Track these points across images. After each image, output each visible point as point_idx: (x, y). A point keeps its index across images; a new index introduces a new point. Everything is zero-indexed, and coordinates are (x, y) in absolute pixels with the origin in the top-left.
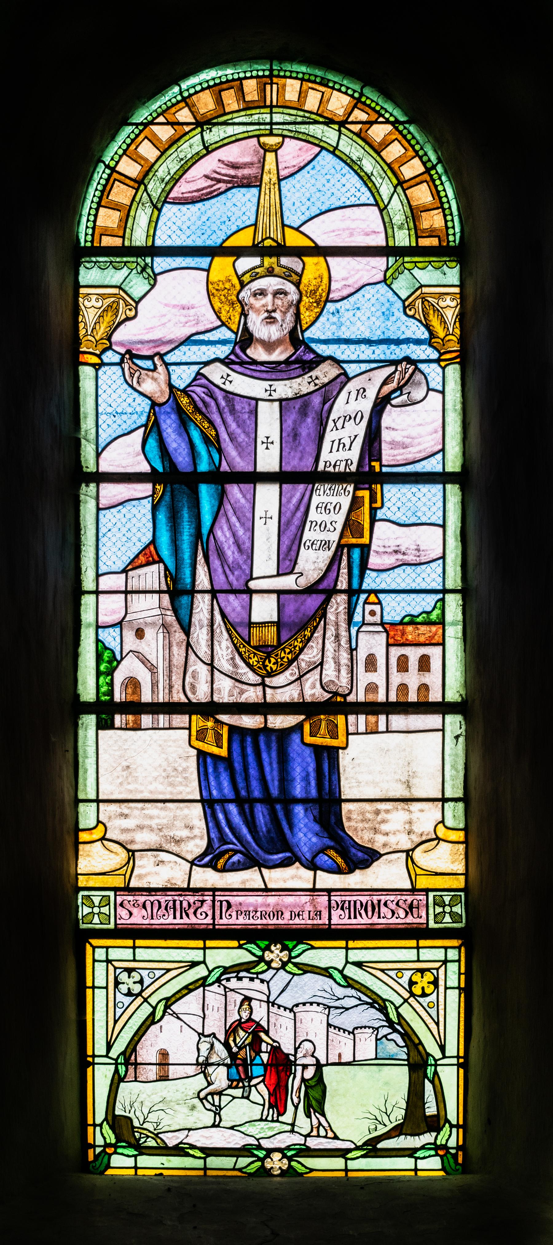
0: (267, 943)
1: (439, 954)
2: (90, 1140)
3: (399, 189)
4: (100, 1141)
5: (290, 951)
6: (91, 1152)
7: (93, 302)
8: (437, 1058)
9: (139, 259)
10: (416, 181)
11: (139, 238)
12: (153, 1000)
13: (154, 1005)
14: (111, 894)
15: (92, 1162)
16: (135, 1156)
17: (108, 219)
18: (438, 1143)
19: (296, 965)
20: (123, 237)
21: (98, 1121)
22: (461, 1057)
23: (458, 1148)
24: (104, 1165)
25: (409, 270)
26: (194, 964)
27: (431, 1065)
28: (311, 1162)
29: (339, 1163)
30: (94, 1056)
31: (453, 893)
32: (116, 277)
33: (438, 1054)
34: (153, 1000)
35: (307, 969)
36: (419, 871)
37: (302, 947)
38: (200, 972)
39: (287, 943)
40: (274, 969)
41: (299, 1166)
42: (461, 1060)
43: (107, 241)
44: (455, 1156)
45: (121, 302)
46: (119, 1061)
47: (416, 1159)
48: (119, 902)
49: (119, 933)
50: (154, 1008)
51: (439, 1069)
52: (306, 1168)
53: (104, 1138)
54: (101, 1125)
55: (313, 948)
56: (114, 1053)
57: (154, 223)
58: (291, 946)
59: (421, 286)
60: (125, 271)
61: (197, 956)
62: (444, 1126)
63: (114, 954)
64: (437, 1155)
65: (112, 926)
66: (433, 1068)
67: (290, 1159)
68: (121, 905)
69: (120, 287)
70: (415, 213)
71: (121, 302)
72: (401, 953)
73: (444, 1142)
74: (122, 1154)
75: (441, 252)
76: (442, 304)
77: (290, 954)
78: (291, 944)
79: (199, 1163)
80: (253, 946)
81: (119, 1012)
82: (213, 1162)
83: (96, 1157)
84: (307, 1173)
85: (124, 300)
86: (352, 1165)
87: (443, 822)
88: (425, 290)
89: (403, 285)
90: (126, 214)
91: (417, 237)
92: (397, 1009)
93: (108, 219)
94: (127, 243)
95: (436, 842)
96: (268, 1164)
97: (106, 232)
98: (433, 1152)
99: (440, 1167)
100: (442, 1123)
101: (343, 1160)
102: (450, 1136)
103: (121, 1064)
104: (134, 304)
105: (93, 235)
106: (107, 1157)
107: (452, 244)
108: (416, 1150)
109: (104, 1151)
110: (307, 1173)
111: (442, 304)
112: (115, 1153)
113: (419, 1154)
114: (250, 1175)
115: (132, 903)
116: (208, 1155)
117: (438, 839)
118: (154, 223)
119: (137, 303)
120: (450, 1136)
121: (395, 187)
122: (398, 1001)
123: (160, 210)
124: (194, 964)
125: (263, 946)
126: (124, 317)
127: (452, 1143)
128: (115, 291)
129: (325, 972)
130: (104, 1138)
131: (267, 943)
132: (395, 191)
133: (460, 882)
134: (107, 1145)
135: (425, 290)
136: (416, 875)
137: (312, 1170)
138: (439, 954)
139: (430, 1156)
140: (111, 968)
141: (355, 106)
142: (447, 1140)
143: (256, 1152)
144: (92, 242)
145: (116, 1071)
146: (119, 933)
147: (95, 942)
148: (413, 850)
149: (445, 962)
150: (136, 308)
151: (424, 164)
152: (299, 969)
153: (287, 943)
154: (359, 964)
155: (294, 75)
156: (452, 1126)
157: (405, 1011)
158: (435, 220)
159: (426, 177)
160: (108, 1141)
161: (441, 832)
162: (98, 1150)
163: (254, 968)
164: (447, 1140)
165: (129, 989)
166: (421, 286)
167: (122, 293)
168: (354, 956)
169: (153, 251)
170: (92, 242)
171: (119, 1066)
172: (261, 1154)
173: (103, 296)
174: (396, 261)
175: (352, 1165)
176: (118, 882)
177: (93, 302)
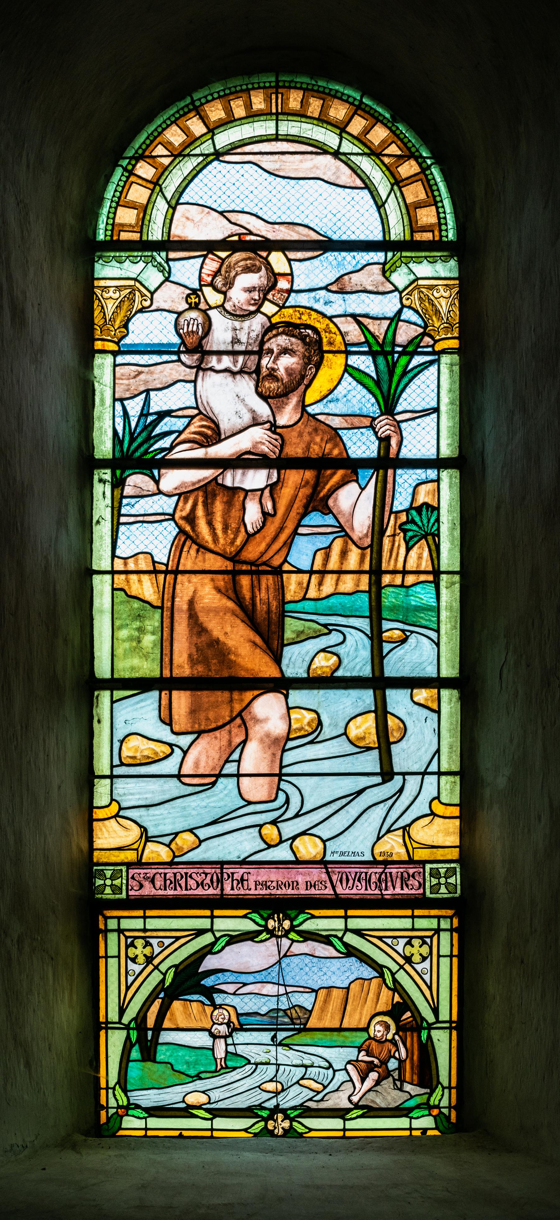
0: (269, 912)
1: (433, 923)
2: (103, 1102)
3: (395, 188)
4: (112, 1103)
5: (292, 921)
6: (103, 1113)
7: (111, 294)
8: (430, 1021)
9: (155, 253)
10: (412, 179)
11: (156, 234)
12: (163, 967)
13: (164, 971)
14: (124, 869)
15: (104, 1124)
16: (145, 1118)
17: (126, 216)
18: (431, 1103)
19: (299, 933)
20: (141, 232)
21: (112, 1084)
22: (454, 1022)
23: (450, 1107)
24: (117, 1126)
25: (406, 264)
26: (200, 932)
27: (425, 1029)
28: (311, 1123)
29: (337, 1123)
30: (107, 1022)
31: (448, 866)
32: (131, 269)
33: (431, 1018)
34: (163, 967)
35: (308, 936)
36: (415, 845)
37: (302, 917)
38: (208, 938)
39: (289, 912)
40: (265, 1109)
41: (300, 1126)
42: (454, 1025)
43: (124, 236)
44: (448, 1118)
45: (137, 293)
46: (131, 1026)
47: (411, 1118)
48: (130, 876)
49: (130, 904)
50: (164, 975)
51: (434, 1033)
52: (306, 1127)
53: (117, 1100)
54: (114, 1089)
55: (313, 917)
56: (126, 1020)
57: (169, 221)
58: (293, 915)
59: (417, 279)
60: (142, 265)
61: (205, 924)
62: (437, 1087)
63: (126, 924)
64: (430, 1115)
65: (124, 895)
66: (426, 1031)
67: (292, 1120)
68: (133, 878)
69: (135, 280)
70: (410, 211)
71: (137, 293)
72: (398, 922)
73: (437, 1103)
74: (133, 1116)
75: (436, 247)
76: (106, 295)
77: (292, 923)
78: (293, 913)
79: (207, 1124)
80: (256, 915)
81: (130, 979)
82: (219, 1123)
83: (108, 1119)
84: (306, 1133)
85: (139, 291)
86: (350, 1125)
87: (438, 798)
88: (421, 282)
89: (401, 278)
90: (144, 210)
91: (412, 231)
92: (393, 974)
93: (126, 216)
94: (145, 238)
95: (431, 817)
96: (271, 1125)
97: (123, 227)
98: (427, 1112)
99: (434, 1126)
100: (435, 1083)
101: (341, 1121)
102: (442, 1095)
103: (133, 1029)
104: (149, 295)
105: (112, 230)
106: (119, 1118)
107: (444, 239)
108: (411, 1109)
109: (117, 1113)
110: (306, 1133)
111: (106, 295)
112: (127, 1115)
113: (414, 1114)
114: (256, 1135)
115: (142, 876)
116: (215, 1116)
117: (433, 814)
118: (169, 221)
119: (152, 294)
120: (442, 1095)
121: (392, 185)
122: (394, 967)
123: (174, 209)
124: (200, 932)
125: (265, 915)
126: (140, 307)
127: (445, 1103)
128: (132, 283)
129: (326, 940)
130: (117, 1100)
131: (269, 912)
132: (392, 189)
133: (454, 854)
134: (119, 1107)
135: (421, 282)
136: (413, 848)
137: (311, 1130)
138: (433, 923)
139: (423, 1116)
140: (122, 938)
141: (355, 113)
142: (440, 1100)
143: (260, 1113)
144: (112, 236)
145: (128, 1037)
146: (130, 904)
147: (108, 913)
148: (409, 825)
149: (438, 931)
150: (152, 300)
151: (420, 165)
152: (301, 937)
153: (289, 912)
154: (358, 932)
155: (298, 85)
156: (444, 1088)
157: (401, 977)
158: (427, 216)
159: (422, 176)
160: (121, 1103)
161: (438, 808)
162: (112, 1111)
163: (257, 937)
164: (440, 1100)
165: (144, 948)
166: (417, 279)
167: (138, 284)
168: (353, 924)
169: (168, 245)
170: (112, 236)
171: (131, 1032)
172: (265, 1114)
173: (119, 288)
174: (394, 256)
175: (350, 1125)
176: (131, 856)
177: (111, 294)
